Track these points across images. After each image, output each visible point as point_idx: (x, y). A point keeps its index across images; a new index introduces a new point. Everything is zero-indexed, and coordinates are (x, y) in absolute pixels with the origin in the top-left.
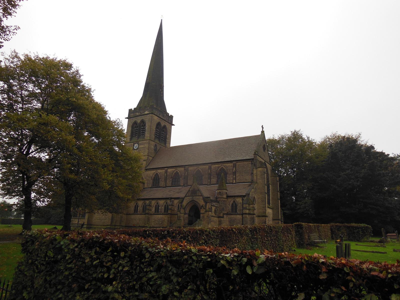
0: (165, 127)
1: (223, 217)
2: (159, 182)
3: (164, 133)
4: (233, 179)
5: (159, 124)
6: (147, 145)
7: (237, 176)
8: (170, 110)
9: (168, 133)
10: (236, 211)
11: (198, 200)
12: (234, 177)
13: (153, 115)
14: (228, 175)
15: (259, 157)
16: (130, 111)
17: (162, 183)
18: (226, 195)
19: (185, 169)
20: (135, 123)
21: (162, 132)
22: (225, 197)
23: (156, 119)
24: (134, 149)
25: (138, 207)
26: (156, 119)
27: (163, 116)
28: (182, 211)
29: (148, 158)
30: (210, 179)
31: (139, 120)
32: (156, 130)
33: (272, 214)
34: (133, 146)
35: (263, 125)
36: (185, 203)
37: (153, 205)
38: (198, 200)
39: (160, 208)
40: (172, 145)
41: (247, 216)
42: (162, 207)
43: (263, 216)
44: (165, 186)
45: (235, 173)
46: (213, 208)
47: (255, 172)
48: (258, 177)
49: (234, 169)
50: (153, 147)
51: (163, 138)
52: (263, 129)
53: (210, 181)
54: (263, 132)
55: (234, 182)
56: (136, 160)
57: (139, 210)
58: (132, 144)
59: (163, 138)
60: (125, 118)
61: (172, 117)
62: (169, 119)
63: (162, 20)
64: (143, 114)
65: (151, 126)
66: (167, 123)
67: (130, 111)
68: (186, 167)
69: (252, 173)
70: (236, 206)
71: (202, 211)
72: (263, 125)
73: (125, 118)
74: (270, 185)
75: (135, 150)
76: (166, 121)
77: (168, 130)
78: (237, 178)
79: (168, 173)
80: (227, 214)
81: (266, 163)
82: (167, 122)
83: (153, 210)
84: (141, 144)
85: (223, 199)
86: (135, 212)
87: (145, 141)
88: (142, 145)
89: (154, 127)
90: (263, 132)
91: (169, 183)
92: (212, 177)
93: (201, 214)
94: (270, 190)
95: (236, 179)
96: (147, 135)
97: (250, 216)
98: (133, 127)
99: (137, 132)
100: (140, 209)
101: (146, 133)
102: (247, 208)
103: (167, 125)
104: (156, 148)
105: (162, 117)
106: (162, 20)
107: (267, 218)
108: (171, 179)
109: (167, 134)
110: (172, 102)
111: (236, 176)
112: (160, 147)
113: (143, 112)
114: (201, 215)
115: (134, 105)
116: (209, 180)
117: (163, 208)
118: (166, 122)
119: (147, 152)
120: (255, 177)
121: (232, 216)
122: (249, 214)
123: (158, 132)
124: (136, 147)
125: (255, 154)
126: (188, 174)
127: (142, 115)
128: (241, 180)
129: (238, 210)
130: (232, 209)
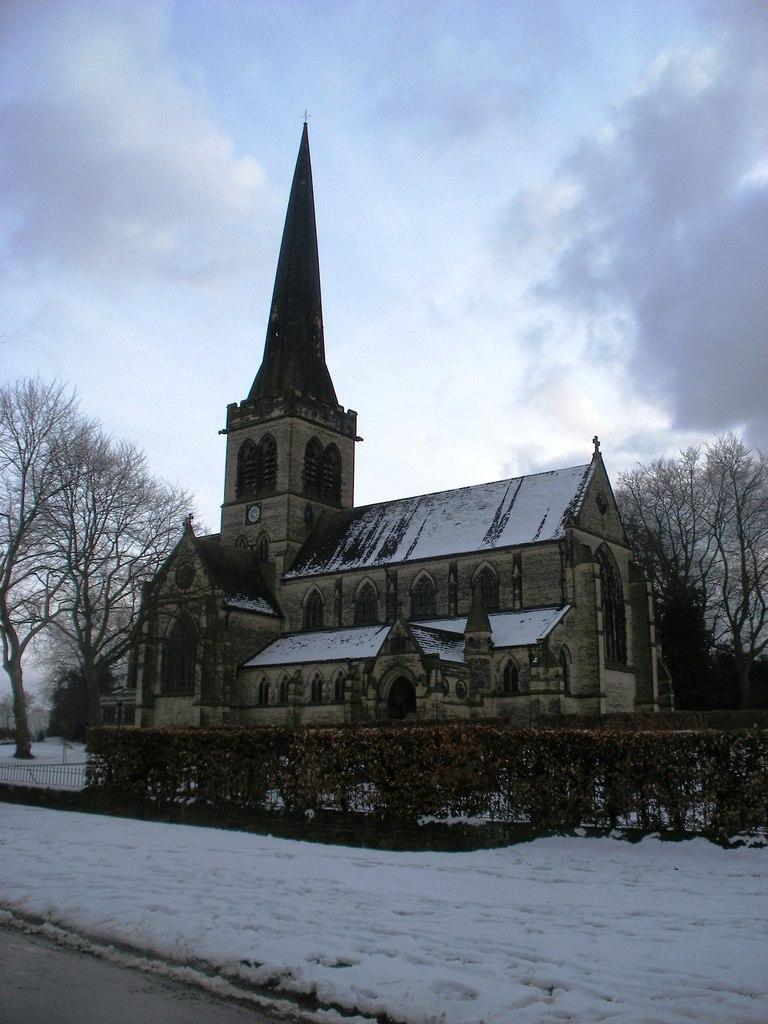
0: (333, 447)
1: (481, 704)
2: (321, 616)
3: (331, 467)
4: (514, 599)
5: (313, 443)
6: (283, 511)
7: (524, 588)
8: (346, 401)
9: (345, 467)
10: (515, 688)
11: (408, 664)
12: (517, 592)
13: (295, 420)
14: (501, 588)
15: (584, 533)
16: (232, 408)
17: (330, 619)
18: (487, 647)
19: (388, 576)
20: (247, 444)
21: (326, 466)
22: (486, 650)
23: (306, 430)
24: (248, 523)
25: (267, 686)
26: (306, 430)
27: (325, 418)
28: (372, 693)
29: (288, 546)
30: (456, 601)
31: (256, 434)
32: (307, 462)
33: (634, 688)
34: (247, 513)
35: (596, 437)
36: (377, 673)
37: (305, 680)
38: (408, 664)
39: (324, 686)
40: (361, 499)
41: (541, 698)
42: (330, 686)
43: (591, 696)
44: (337, 625)
45: (517, 583)
46: (450, 683)
47: (569, 576)
48: (578, 591)
49: (516, 571)
50: (300, 513)
51: (330, 482)
52: (597, 448)
53: (456, 606)
54: (597, 456)
55: (518, 606)
56: (580, 161)
57: (270, 696)
58: (244, 506)
59: (330, 482)
60: (220, 433)
61: (352, 416)
62: (346, 424)
63: (306, 124)
64: (267, 417)
65: (290, 454)
66: (339, 436)
67: (232, 408)
68: (391, 569)
69: (563, 580)
70: (515, 672)
71: (420, 691)
72: (596, 437)
73: (220, 433)
74: (628, 608)
75: (252, 523)
76: (335, 431)
77: (343, 457)
78: (524, 597)
79: (344, 589)
80: (494, 695)
81: (609, 544)
82: (338, 432)
83: (308, 693)
84: (269, 507)
85: (479, 657)
86: (507, 689)
87: (278, 498)
88: (270, 508)
89: (300, 456)
90: (597, 456)
91: (348, 614)
92: (460, 595)
93: (417, 700)
94: (628, 622)
95: (521, 599)
96: (282, 480)
97: (550, 697)
98: (240, 456)
99: (254, 471)
100: (274, 692)
101: (279, 474)
102: (541, 676)
103: (340, 441)
104: (312, 515)
105: (322, 422)
106: (306, 124)
107: (603, 700)
108: (353, 605)
109: (340, 471)
110: (352, 367)
111: (521, 589)
112: (323, 512)
113: (268, 413)
114: (419, 702)
115: (241, 393)
116: (453, 604)
117: (332, 686)
118: (335, 434)
119: (285, 531)
120: (570, 590)
121: (507, 700)
122: (546, 692)
123: (313, 467)
124: (255, 511)
125: (566, 523)
126: (395, 589)
127: (263, 422)
128: (535, 600)
129: (519, 684)
130: (506, 681)
